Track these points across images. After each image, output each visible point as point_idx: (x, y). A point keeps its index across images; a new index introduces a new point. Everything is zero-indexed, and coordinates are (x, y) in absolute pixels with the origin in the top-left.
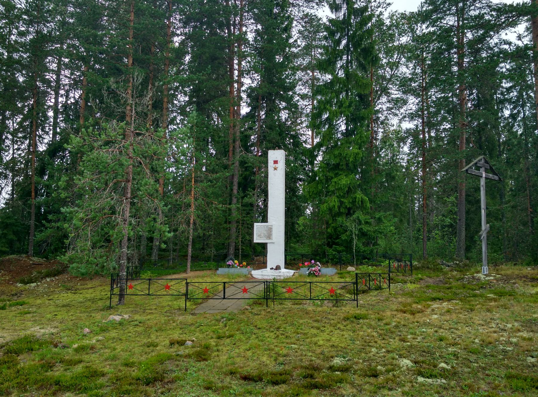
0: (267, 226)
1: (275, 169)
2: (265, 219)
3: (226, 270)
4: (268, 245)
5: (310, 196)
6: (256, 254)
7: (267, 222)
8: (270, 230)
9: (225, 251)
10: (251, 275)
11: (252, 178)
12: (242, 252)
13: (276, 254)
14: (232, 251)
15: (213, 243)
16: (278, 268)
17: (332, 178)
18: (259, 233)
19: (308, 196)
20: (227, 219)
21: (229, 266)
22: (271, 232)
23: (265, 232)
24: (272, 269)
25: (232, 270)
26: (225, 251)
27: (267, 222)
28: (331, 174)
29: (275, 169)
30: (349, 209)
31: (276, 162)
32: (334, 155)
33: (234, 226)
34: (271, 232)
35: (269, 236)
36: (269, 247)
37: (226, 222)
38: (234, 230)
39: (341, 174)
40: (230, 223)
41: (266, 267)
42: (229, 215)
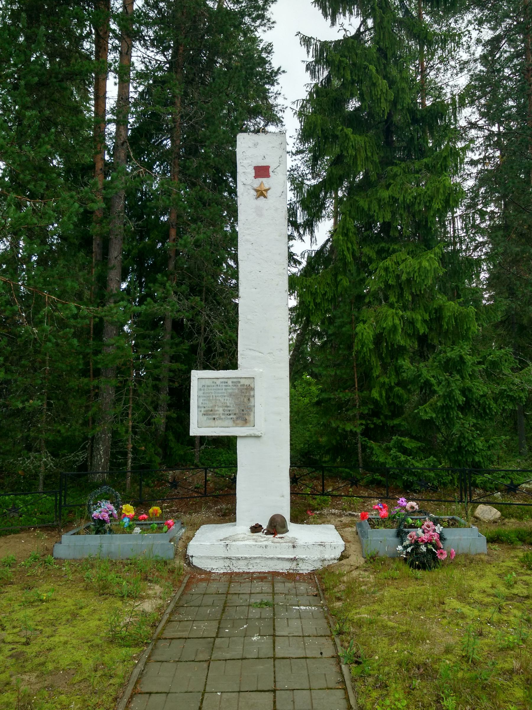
0: (236, 382)
1: (261, 193)
2: (225, 356)
3: (92, 543)
4: (240, 445)
5: (316, 304)
6: (206, 479)
7: (234, 366)
8: (245, 393)
9: (82, 456)
10: (186, 558)
11: (267, 87)
12: (134, 459)
13: (264, 475)
14: (102, 457)
15: (43, 436)
16: (276, 527)
17: (371, 261)
18: (209, 405)
19: (312, 304)
20: (87, 364)
21: (100, 527)
22: (253, 399)
23: (229, 401)
24: (256, 529)
25: (116, 544)
26: (82, 456)
27: (234, 366)
28: (368, 251)
29: (261, 193)
30: (423, 340)
31: (262, 172)
32: (379, 201)
33: (107, 385)
34: (253, 399)
35: (243, 414)
36: (244, 452)
37: (85, 373)
38: (108, 395)
39: (394, 251)
40: (97, 373)
41: (228, 515)
42: (96, 353)
